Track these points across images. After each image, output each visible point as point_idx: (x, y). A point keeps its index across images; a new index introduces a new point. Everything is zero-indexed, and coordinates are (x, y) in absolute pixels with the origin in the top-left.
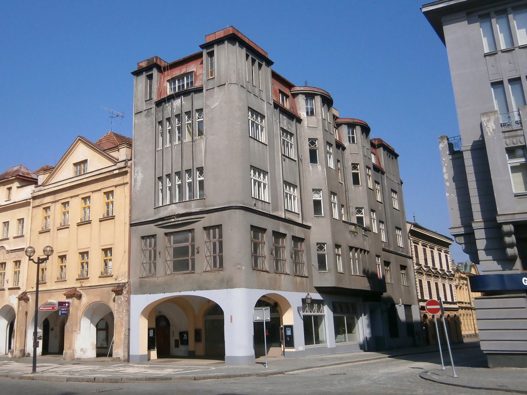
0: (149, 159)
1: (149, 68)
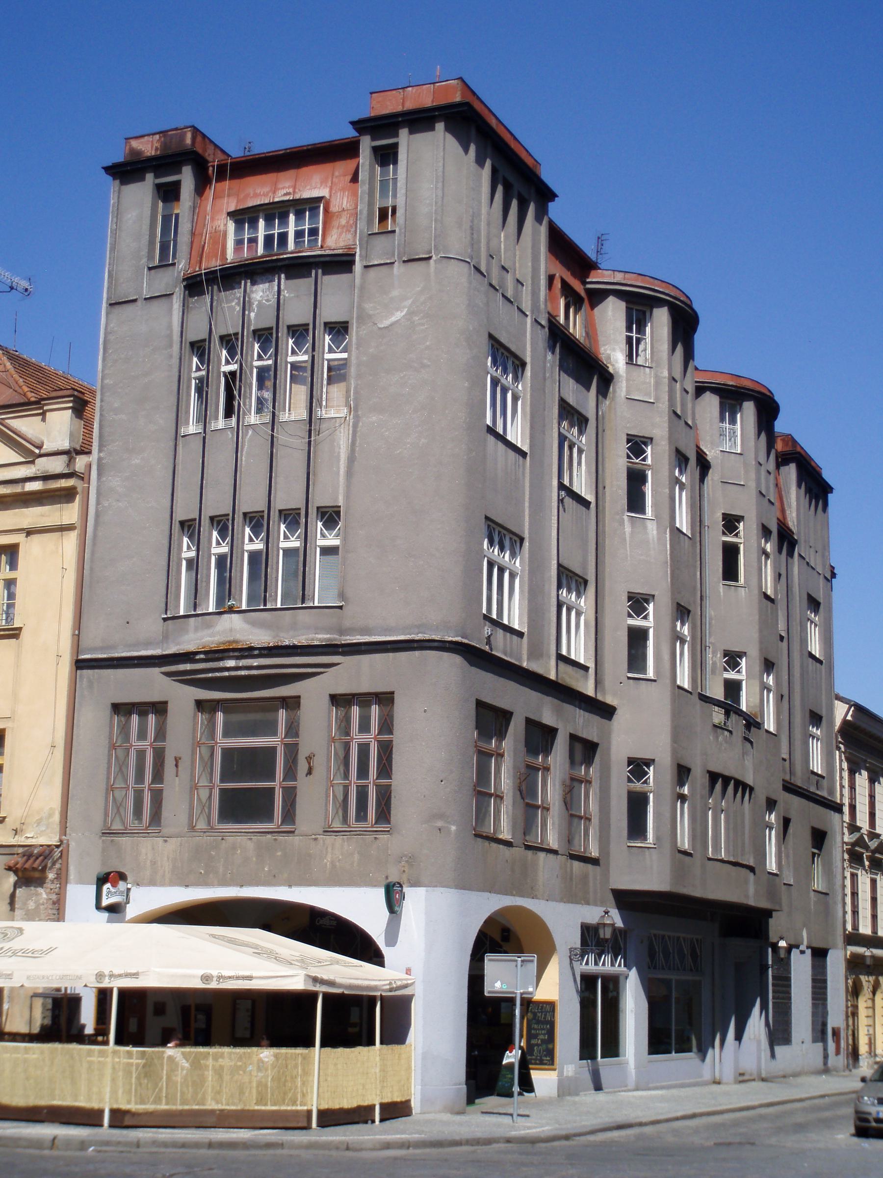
0: (152, 459)
1: (167, 162)
